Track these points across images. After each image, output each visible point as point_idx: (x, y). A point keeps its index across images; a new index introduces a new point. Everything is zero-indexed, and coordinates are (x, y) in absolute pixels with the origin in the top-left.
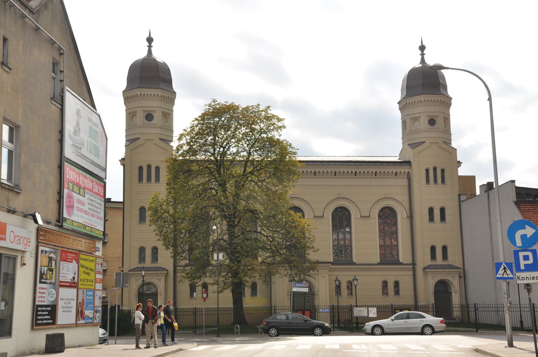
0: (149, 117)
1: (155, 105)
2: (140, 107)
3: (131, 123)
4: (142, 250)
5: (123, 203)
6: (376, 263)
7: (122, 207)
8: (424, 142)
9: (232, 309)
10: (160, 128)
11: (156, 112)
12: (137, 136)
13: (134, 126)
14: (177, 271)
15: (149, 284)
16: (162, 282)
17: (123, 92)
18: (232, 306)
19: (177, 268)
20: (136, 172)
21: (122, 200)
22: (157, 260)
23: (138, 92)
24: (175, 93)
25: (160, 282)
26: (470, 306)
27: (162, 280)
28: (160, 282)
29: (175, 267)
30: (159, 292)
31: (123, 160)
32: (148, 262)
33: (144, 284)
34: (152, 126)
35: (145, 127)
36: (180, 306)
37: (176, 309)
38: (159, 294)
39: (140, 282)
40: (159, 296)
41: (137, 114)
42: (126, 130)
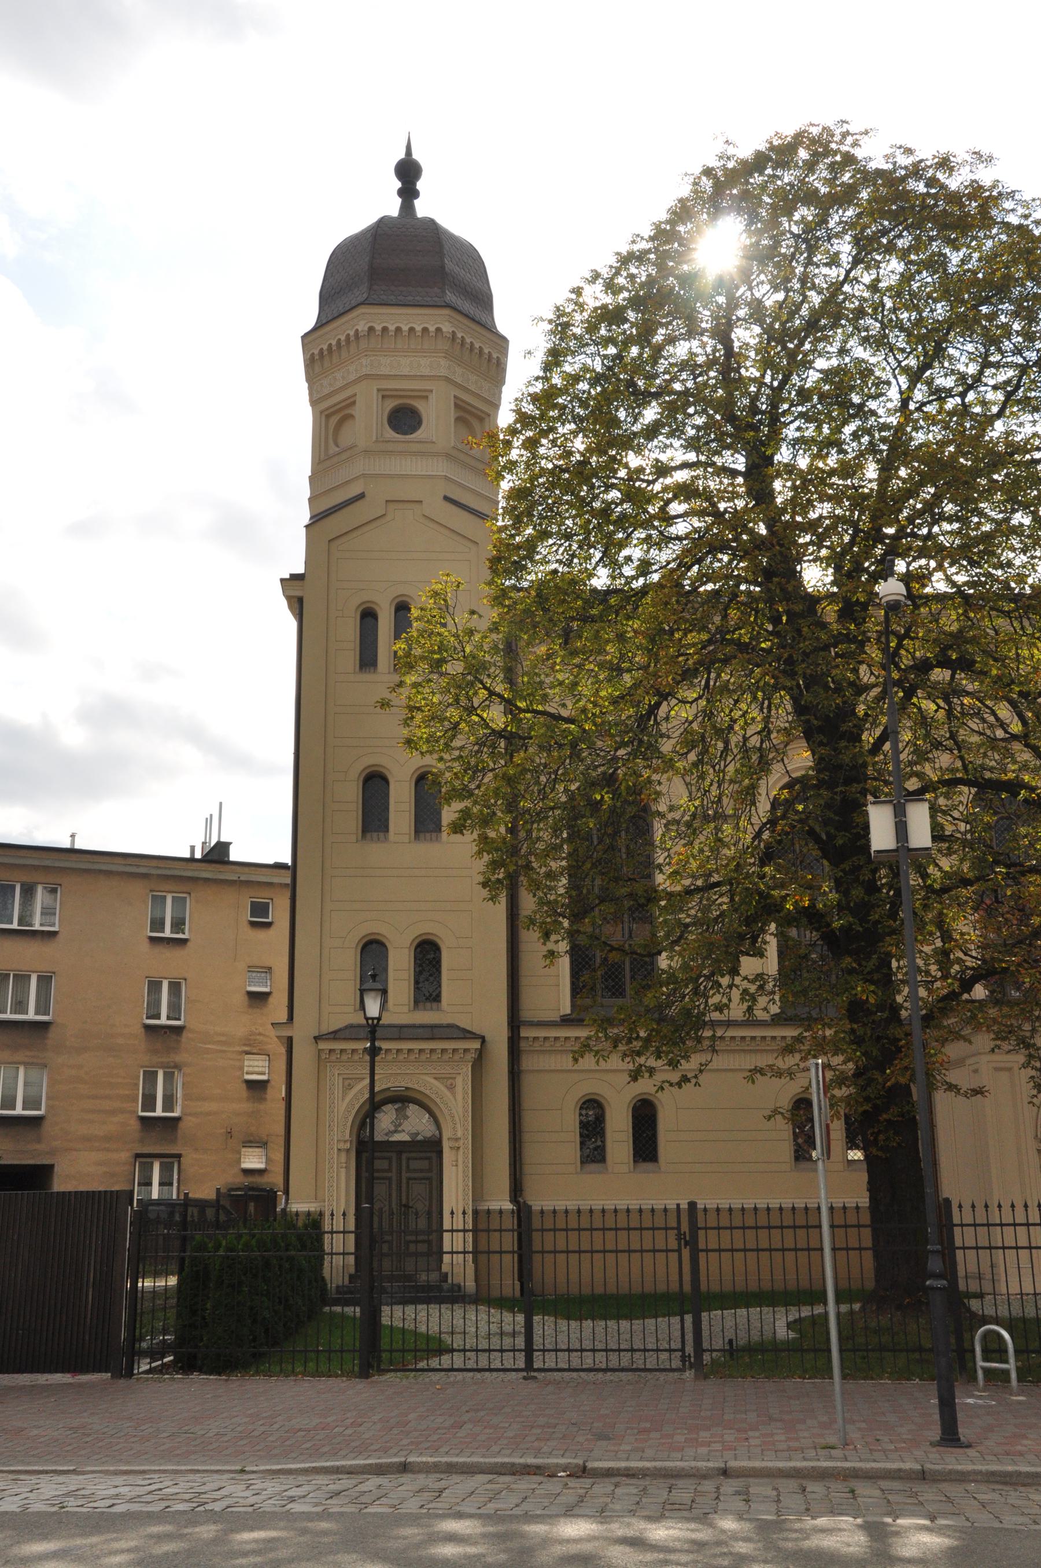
0: (404, 419)
1: (426, 372)
2: (367, 377)
3: (333, 449)
4: (373, 950)
5: (287, 876)
6: (555, 1017)
7: (288, 881)
8: (362, 496)
9: (866, 1218)
10: (448, 456)
11: (432, 398)
12: (354, 490)
13: (344, 456)
14: (523, 1045)
15: (402, 1099)
16: (459, 1089)
17: (304, 337)
18: (864, 1201)
19: (524, 1033)
20: (349, 630)
21: (287, 860)
22: (436, 998)
23: (361, 320)
24: (505, 340)
25: (451, 1088)
26: (536, 1223)
27: (459, 1081)
28: (451, 1088)
29: (515, 1022)
30: (445, 1136)
31: (292, 584)
32: (398, 1004)
33: (374, 1105)
34: (415, 447)
35: (391, 453)
36: (539, 1201)
37: (523, 1213)
38: (446, 1145)
39: (360, 1091)
40: (447, 1156)
41: (358, 411)
42: (311, 479)
